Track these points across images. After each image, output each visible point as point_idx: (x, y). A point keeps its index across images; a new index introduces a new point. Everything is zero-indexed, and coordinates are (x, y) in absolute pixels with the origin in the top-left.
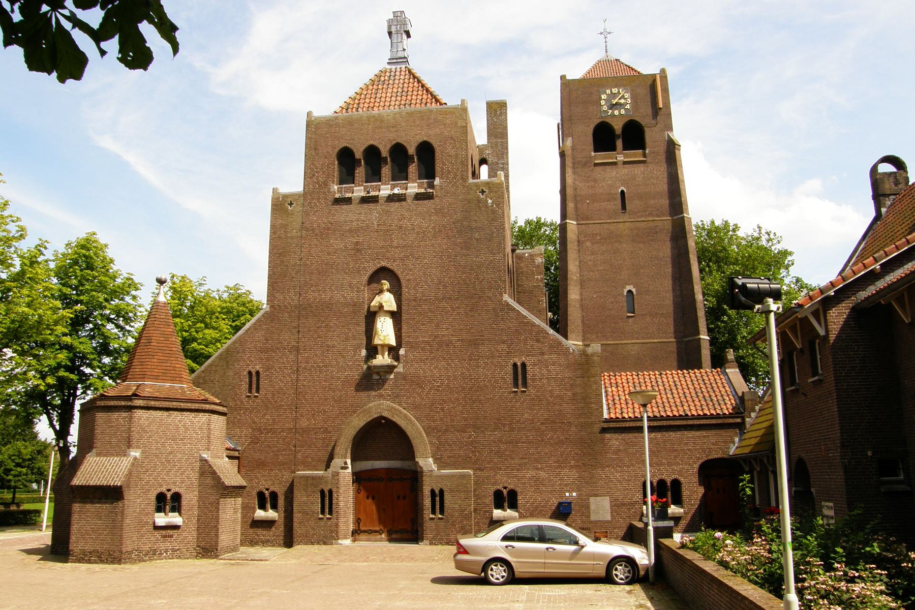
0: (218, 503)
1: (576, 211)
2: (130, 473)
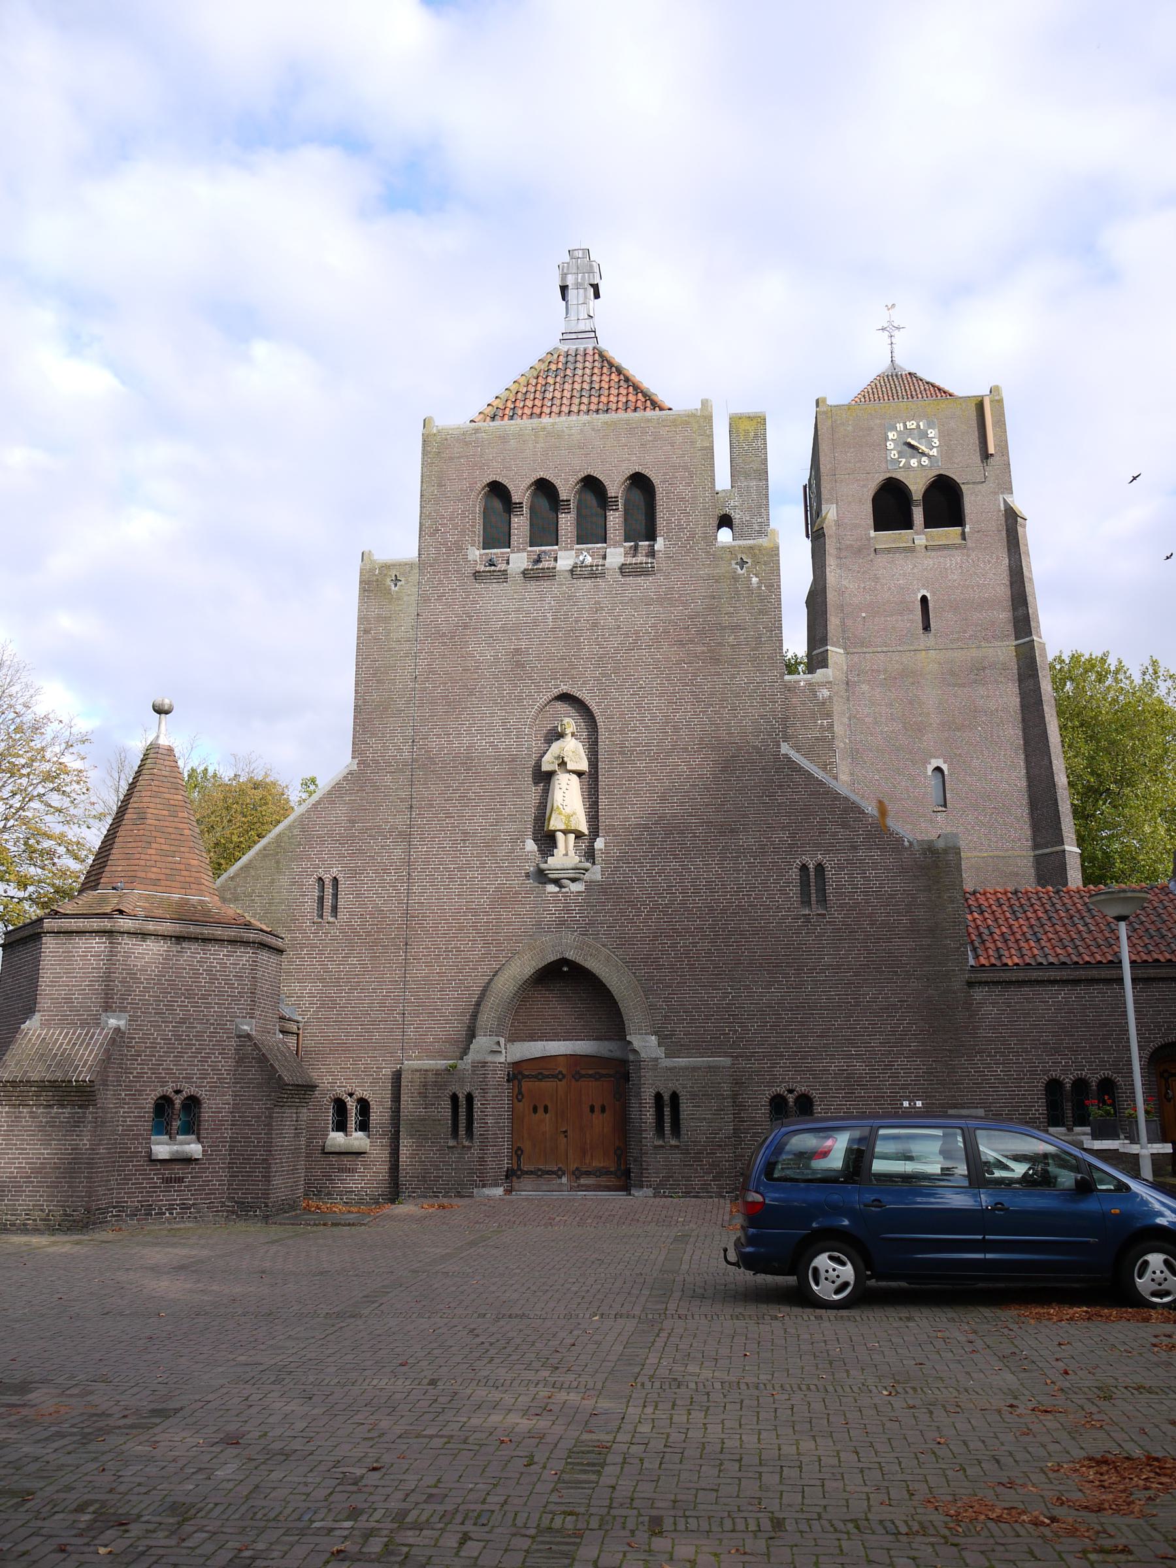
1: (844, 631)
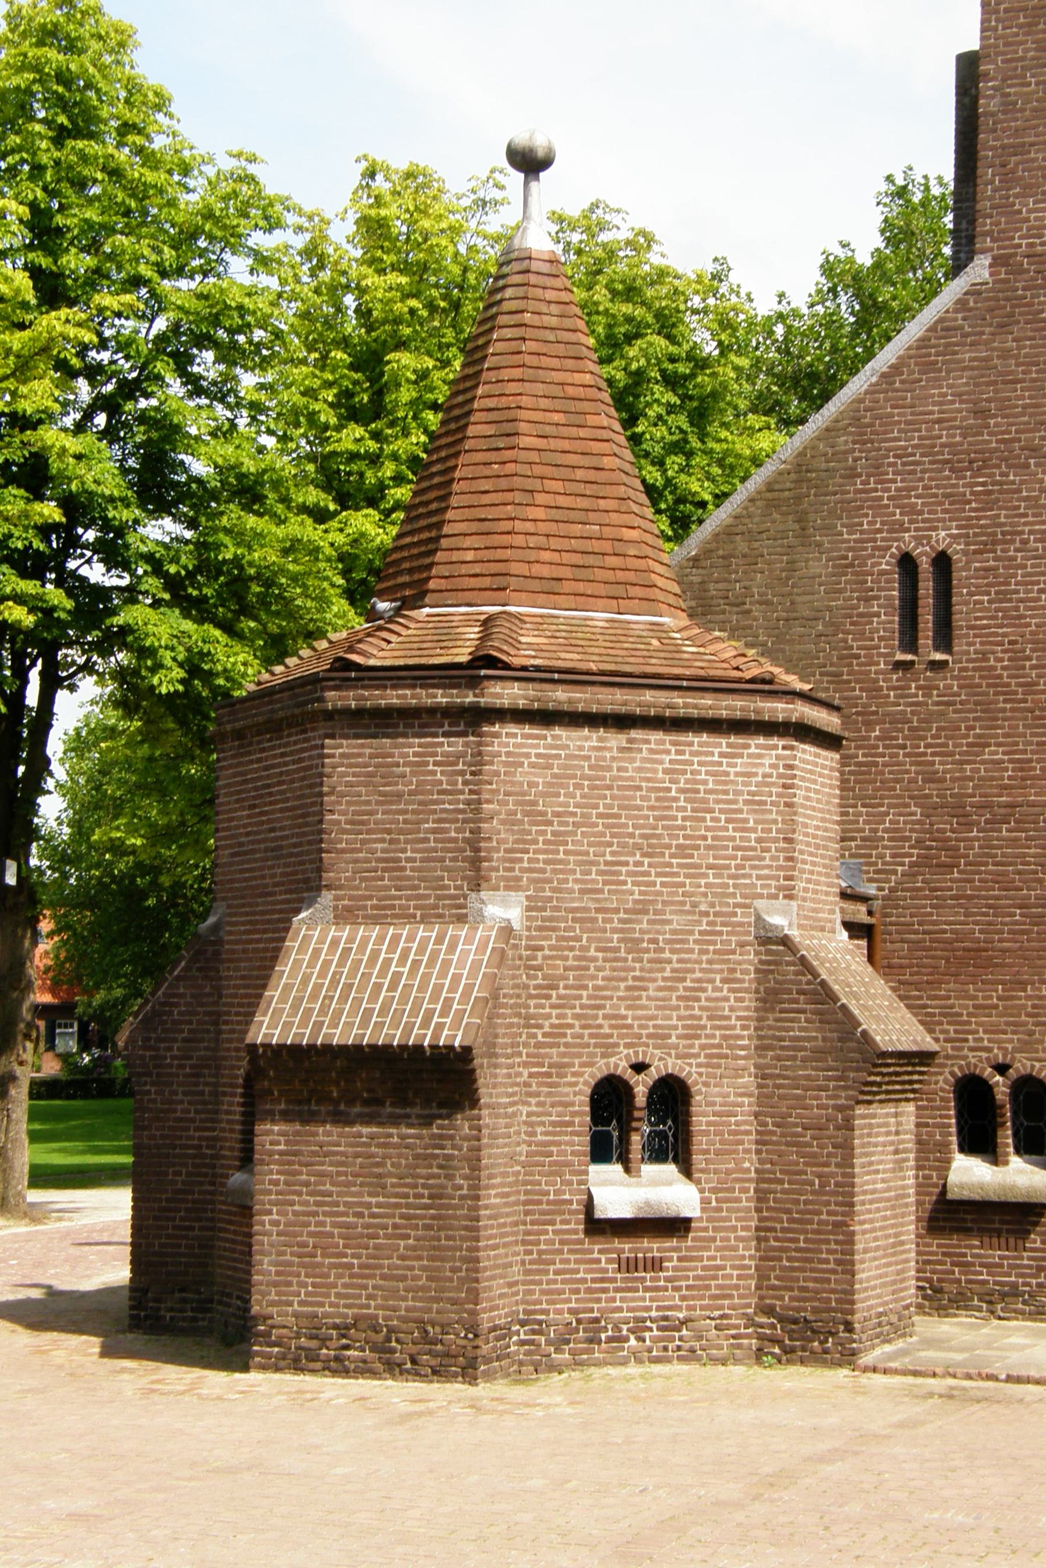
0: (848, 1126)
2: (494, 997)
